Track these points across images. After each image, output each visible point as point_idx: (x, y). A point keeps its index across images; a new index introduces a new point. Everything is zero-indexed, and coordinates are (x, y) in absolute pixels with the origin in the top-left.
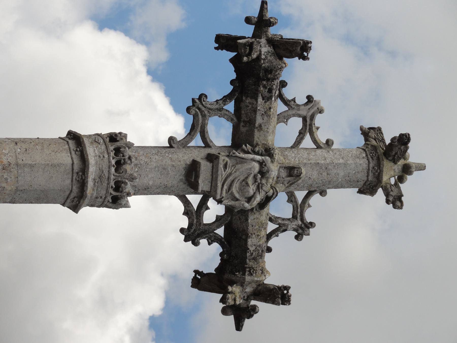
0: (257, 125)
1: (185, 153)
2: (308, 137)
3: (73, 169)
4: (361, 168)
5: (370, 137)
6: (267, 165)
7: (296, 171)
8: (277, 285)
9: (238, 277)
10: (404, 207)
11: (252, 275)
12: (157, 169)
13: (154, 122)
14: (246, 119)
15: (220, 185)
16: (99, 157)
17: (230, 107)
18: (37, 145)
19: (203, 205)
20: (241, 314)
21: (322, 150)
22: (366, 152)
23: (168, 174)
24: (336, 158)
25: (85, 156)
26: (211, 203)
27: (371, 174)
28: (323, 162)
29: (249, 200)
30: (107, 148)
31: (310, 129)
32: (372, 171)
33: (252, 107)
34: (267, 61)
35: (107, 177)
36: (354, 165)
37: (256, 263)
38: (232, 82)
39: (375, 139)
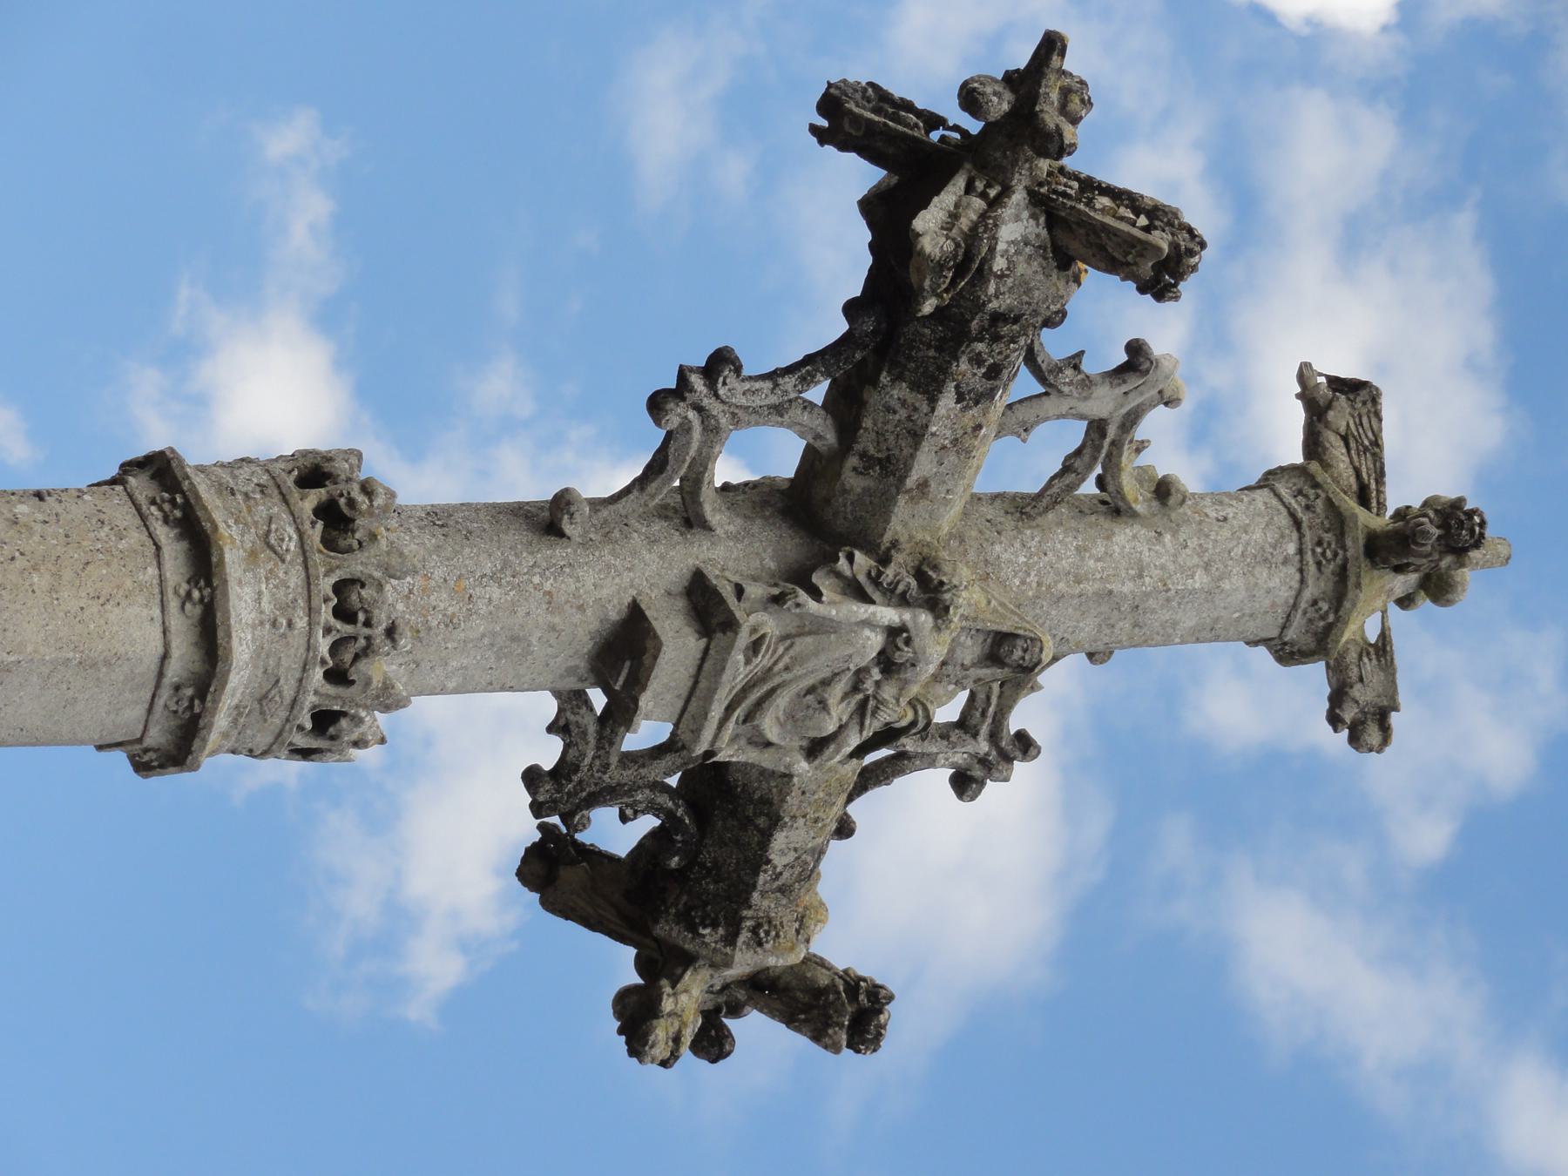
0: (910, 482)
1: (609, 566)
3: (161, 674)
4: (1267, 603)
5: (1327, 425)
6: (916, 642)
7: (1018, 653)
8: (840, 965)
9: (707, 945)
10: (1388, 750)
11: (760, 944)
12: (486, 641)
14: (872, 451)
15: (716, 712)
16: (274, 624)
18: (35, 568)
21: (1137, 527)
22: (1301, 537)
23: (527, 652)
24: (1182, 569)
25: (220, 634)
27: (1298, 620)
28: (1128, 588)
30: (308, 582)
31: (1109, 455)
32: (1305, 613)
33: (909, 418)
34: (1010, 281)
35: (288, 701)
36: (1242, 595)
37: (784, 902)
39: (1345, 439)
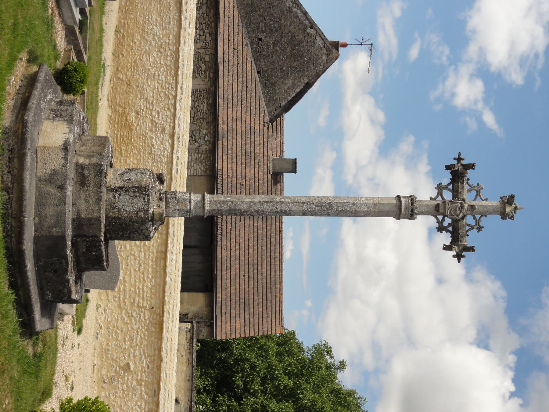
2: (478, 197)
13: (426, 193)
17: (451, 187)
19: (443, 219)
26: (446, 218)
29: (458, 216)
38: (451, 179)
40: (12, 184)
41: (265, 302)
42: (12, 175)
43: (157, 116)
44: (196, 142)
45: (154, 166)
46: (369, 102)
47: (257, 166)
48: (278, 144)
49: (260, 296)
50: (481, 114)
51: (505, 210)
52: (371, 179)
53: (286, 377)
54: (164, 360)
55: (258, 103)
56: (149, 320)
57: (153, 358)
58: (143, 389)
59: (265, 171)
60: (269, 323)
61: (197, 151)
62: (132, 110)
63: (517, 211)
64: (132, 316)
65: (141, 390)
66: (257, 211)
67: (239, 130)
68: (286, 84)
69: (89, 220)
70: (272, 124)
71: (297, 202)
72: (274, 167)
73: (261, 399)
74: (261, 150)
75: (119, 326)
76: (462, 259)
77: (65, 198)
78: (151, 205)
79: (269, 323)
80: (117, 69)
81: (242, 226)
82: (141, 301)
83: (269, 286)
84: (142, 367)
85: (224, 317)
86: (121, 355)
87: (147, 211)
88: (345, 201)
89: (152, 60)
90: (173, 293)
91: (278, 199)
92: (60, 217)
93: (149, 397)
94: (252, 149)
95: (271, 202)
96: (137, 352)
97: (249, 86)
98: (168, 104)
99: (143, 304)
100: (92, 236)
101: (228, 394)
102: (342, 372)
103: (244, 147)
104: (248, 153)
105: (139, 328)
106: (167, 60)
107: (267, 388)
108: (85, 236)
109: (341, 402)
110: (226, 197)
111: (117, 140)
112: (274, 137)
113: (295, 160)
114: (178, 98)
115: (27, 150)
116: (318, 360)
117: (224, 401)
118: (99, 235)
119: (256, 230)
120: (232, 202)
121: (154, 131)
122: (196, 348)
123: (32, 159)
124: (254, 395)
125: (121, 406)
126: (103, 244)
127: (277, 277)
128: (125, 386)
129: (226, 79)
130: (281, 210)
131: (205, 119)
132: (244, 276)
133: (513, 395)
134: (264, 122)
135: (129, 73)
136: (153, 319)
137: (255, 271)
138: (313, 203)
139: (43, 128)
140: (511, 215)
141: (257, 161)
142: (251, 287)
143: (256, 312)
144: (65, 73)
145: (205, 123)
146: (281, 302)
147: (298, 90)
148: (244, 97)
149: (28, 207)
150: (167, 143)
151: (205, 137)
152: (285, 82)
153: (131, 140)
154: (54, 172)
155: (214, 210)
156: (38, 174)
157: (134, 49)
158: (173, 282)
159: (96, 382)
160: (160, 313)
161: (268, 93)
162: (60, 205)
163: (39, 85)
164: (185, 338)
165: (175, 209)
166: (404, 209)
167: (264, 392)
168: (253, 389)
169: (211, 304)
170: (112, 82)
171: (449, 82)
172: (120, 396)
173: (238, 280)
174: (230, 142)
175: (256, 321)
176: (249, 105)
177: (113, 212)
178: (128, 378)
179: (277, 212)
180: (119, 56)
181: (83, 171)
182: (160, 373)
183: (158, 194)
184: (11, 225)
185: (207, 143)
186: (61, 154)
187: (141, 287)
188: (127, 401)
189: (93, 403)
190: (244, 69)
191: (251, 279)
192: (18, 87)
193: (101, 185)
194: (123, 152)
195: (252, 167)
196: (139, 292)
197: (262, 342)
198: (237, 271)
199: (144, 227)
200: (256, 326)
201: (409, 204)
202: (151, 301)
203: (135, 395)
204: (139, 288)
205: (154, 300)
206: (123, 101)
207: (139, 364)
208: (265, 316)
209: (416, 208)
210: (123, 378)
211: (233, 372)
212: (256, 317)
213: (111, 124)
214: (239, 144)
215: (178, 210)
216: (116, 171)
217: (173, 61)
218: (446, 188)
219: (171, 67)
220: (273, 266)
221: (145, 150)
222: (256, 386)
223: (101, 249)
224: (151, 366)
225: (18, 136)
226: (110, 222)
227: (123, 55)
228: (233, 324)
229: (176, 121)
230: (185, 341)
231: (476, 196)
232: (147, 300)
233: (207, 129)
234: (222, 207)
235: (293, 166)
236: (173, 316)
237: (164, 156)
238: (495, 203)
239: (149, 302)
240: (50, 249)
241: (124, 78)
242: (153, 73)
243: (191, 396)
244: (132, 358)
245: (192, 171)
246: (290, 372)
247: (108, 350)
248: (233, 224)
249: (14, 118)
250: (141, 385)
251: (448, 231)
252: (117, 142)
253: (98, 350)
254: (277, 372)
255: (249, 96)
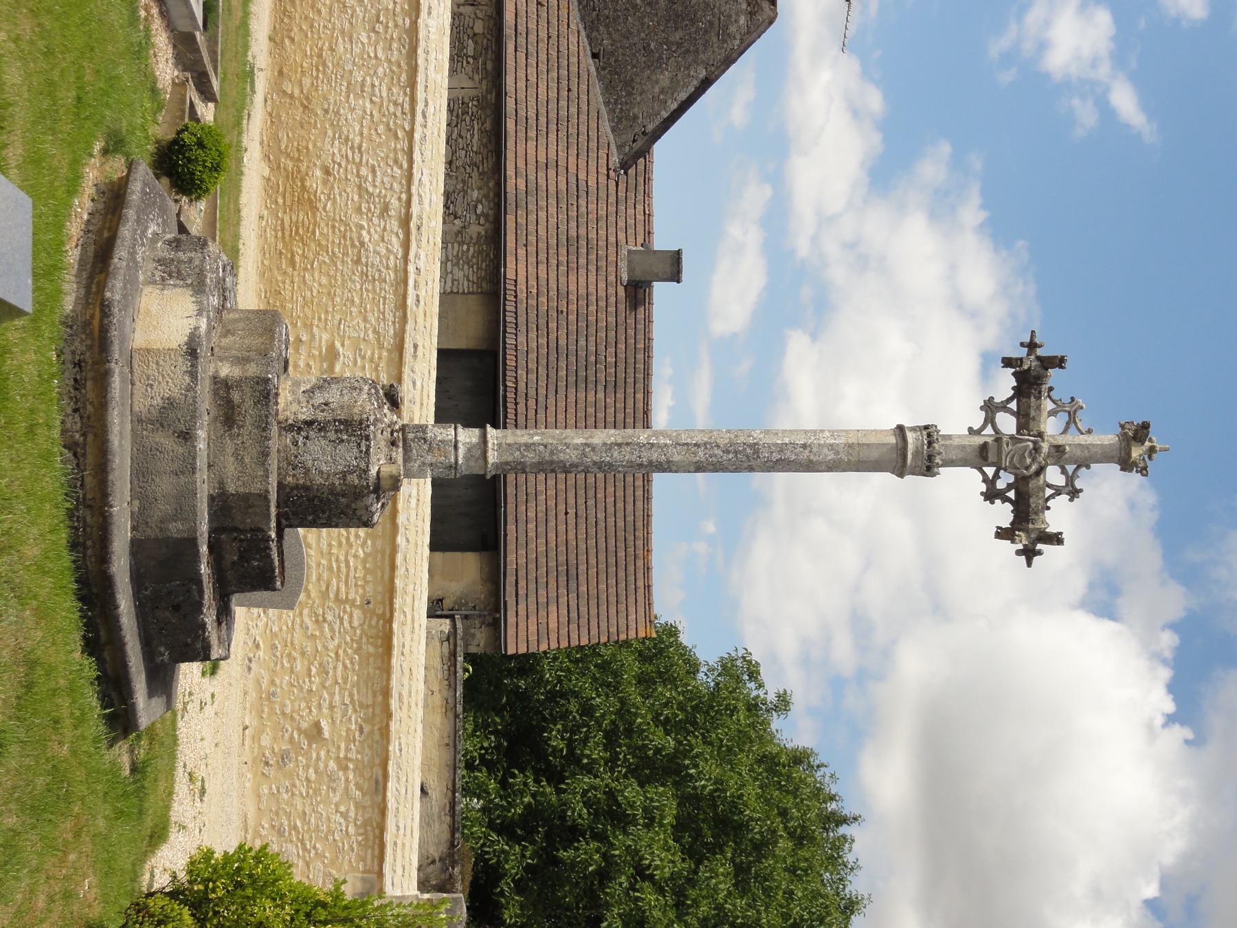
13: (959, 418)
17: (1013, 405)
19: (996, 476)
20: (1029, 554)
29: (1027, 468)
38: (1013, 388)
40: (84, 435)
41: (612, 570)
42: (81, 417)
43: (370, 179)
44: (456, 218)
45: (367, 290)
46: (850, 65)
47: (592, 268)
48: (640, 217)
49: (602, 557)
50: (1107, 90)
51: (1129, 454)
52: (851, 246)
53: (660, 731)
54: (396, 715)
55: (593, 125)
56: (363, 630)
57: (371, 710)
58: (351, 777)
59: (612, 278)
60: (622, 615)
61: (459, 239)
62: (315, 165)
63: (1154, 456)
64: (325, 620)
65: (347, 780)
66: (599, 465)
67: (552, 189)
68: (657, 82)
69: (245, 498)
70: (626, 173)
71: (684, 444)
72: (631, 270)
73: (606, 779)
74: (602, 232)
75: (296, 642)
76: (1036, 559)
77: (194, 458)
78: (373, 458)
79: (622, 615)
80: (281, 73)
81: (561, 404)
82: (343, 588)
83: (621, 534)
84: (348, 730)
85: (522, 607)
86: (303, 705)
87: (366, 471)
88: (787, 440)
89: (357, 50)
90: (412, 571)
91: (643, 436)
92: (184, 509)
93: (364, 795)
94: (582, 231)
95: (628, 444)
96: (337, 697)
97: (574, 89)
98: (395, 149)
99: (347, 593)
100: (252, 530)
101: (533, 768)
102: (782, 717)
103: (563, 228)
104: (573, 241)
105: (339, 646)
106: (390, 49)
107: (618, 754)
108: (236, 529)
109: (779, 783)
110: (532, 436)
111: (283, 233)
112: (631, 202)
113: (679, 253)
114: (417, 136)
115: (113, 365)
116: (731, 692)
117: (525, 784)
118: (265, 528)
119: (591, 410)
120: (546, 446)
121: (364, 210)
122: (462, 676)
123: (123, 381)
124: (589, 770)
125: (305, 813)
126: (273, 545)
127: (639, 513)
128: (311, 770)
129: (521, 74)
130: (650, 463)
131: (475, 165)
132: (566, 513)
133: (1170, 720)
134: (608, 169)
135: (307, 82)
136: (370, 626)
137: (591, 502)
138: (718, 446)
139: (143, 305)
140: (1142, 465)
141: (593, 257)
142: (582, 536)
143: (593, 592)
144: (179, 152)
145: (475, 175)
146: (647, 569)
147: (683, 96)
148: (563, 113)
149: (118, 484)
150: (394, 239)
151: (476, 207)
152: (654, 78)
153: (314, 233)
154: (170, 404)
155: (507, 463)
156: (136, 409)
157: (316, 25)
158: (412, 545)
159: (249, 763)
160: (384, 612)
161: (616, 103)
162: (183, 473)
163: (130, 213)
164: (438, 653)
165: (424, 464)
166: (913, 455)
167: (612, 762)
168: (588, 757)
169: (494, 577)
170: (269, 102)
171: (1034, 17)
172: (301, 794)
173: (552, 524)
174: (532, 217)
175: (594, 612)
176: (573, 131)
177: (294, 476)
178: (318, 754)
179: (641, 465)
180: (283, 40)
181: (228, 393)
182: (388, 743)
183: (387, 434)
184: (85, 521)
185: (482, 221)
186: (183, 365)
187: (342, 558)
188: (318, 804)
189: (257, 859)
190: (563, 49)
191: (582, 521)
192: (86, 217)
193: (267, 423)
194: (297, 259)
195: (582, 272)
196: (339, 568)
197: (606, 652)
198: (551, 503)
199: (359, 504)
200: (594, 623)
201: (923, 444)
202: (364, 589)
203: (334, 790)
204: (337, 560)
205: (371, 585)
206: (295, 144)
207: (341, 726)
208: (613, 599)
209: (940, 453)
210: (307, 755)
211: (544, 719)
212: (593, 602)
213: (270, 196)
214: (553, 221)
215: (431, 465)
216: (297, 384)
217: (404, 51)
218: (1003, 407)
219: (399, 66)
220: (630, 491)
221: (346, 254)
222: (595, 751)
223: (269, 556)
224: (367, 729)
225: (92, 332)
226: (288, 496)
227: (292, 40)
228: (543, 621)
229: (414, 189)
230: (439, 659)
231: (1068, 424)
232: (356, 585)
233: (480, 188)
234: (523, 456)
235: (673, 267)
236: (413, 620)
237: (388, 268)
238: (1107, 438)
239: (361, 591)
240: (164, 565)
241: (297, 92)
242: (360, 79)
243: (454, 781)
244: (325, 711)
245: (449, 284)
246: (667, 718)
247: (274, 694)
248: (541, 399)
249: (83, 292)
250: (346, 769)
251: (1006, 500)
252: (283, 237)
253: (253, 695)
254: (639, 720)
255: (573, 110)
